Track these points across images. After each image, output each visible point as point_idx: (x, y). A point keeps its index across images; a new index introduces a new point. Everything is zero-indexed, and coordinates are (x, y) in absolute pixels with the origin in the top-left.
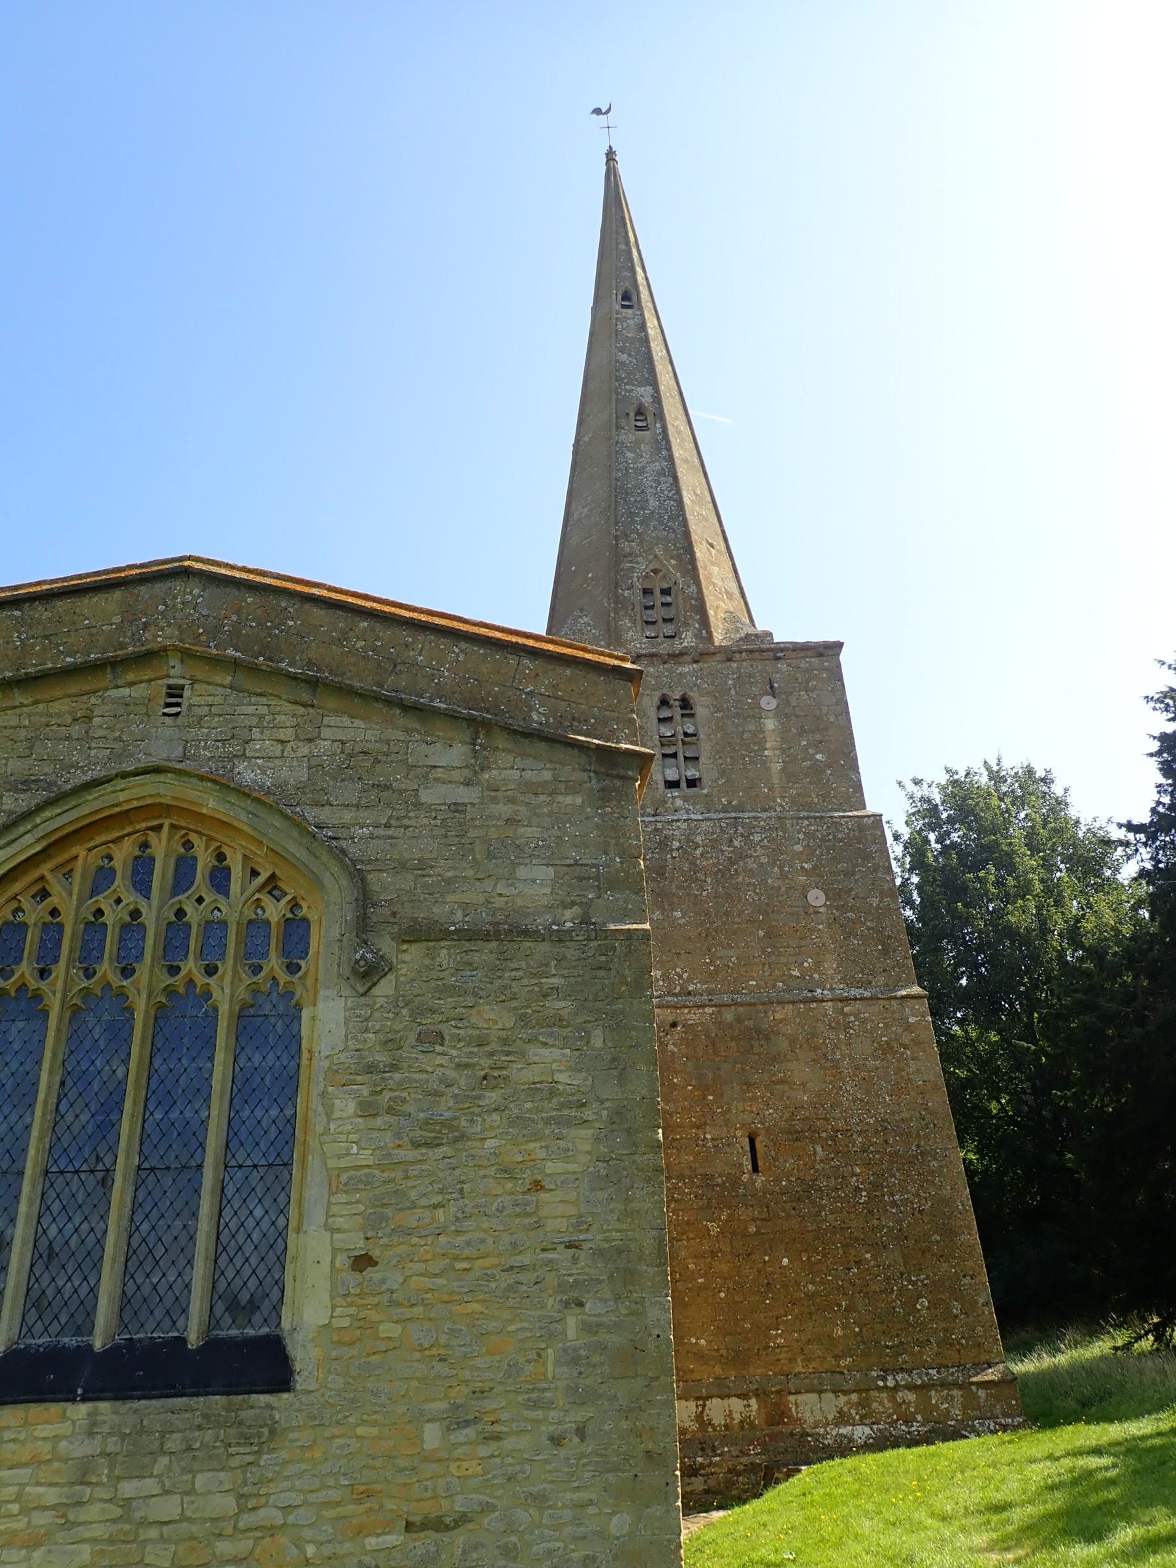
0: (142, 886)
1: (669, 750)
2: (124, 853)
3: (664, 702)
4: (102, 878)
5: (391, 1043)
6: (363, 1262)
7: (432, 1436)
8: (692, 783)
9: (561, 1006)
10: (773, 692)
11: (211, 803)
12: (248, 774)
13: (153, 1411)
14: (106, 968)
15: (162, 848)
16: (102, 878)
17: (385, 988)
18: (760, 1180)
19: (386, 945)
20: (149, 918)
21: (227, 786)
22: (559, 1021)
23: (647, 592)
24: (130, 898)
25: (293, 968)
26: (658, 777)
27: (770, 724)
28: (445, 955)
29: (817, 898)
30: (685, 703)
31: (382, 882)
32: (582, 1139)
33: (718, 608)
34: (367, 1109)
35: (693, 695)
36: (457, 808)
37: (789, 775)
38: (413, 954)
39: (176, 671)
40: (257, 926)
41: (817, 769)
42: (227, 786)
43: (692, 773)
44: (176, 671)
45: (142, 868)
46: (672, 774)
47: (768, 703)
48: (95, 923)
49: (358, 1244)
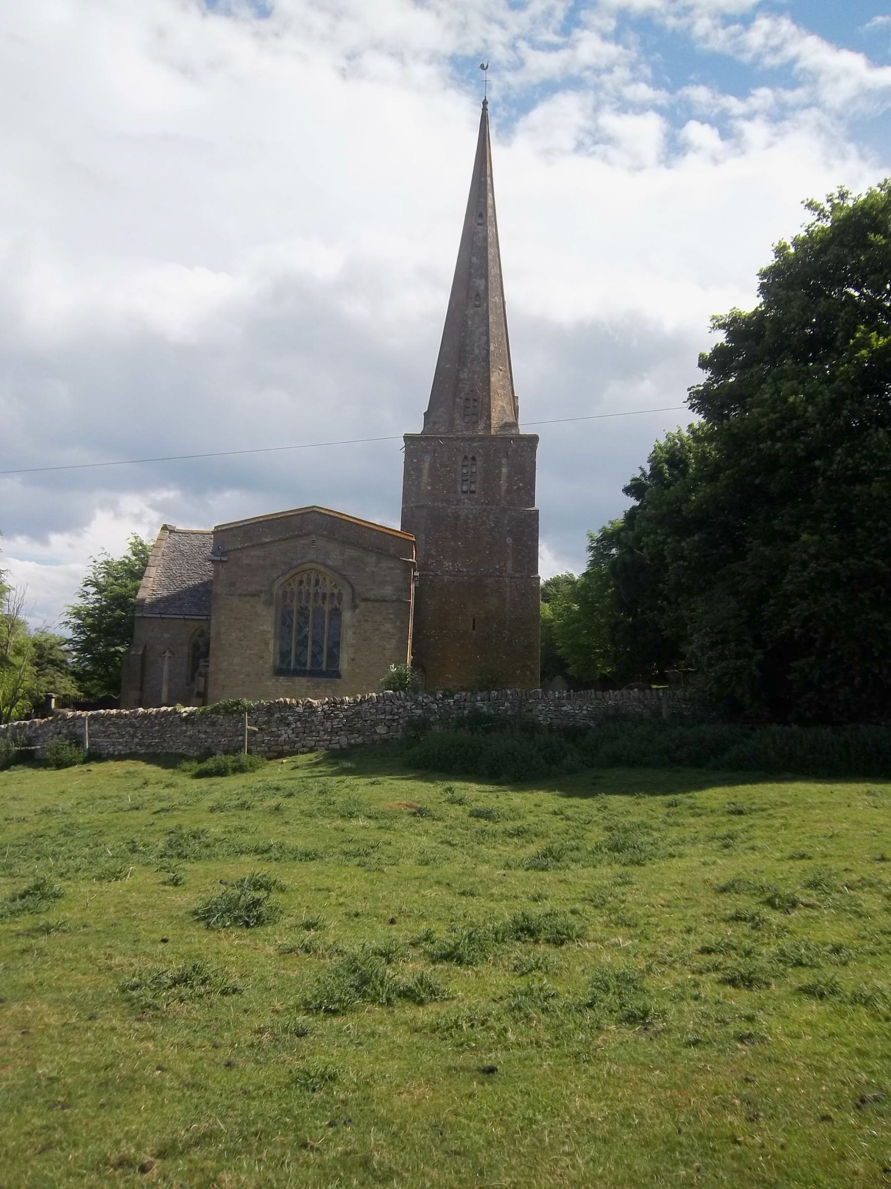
0: (309, 583)
1: (465, 478)
2: (305, 578)
3: (466, 458)
4: (301, 582)
5: (359, 621)
6: (353, 660)
7: (364, 687)
8: (473, 492)
9: (392, 616)
10: (507, 456)
11: (322, 569)
12: (330, 563)
13: (316, 679)
14: (304, 602)
15: (313, 577)
16: (301, 582)
17: (358, 611)
18: (474, 632)
19: (358, 602)
20: (311, 591)
21: (325, 565)
22: (391, 619)
23: (467, 400)
24: (307, 588)
25: (339, 603)
26: (459, 490)
27: (504, 470)
28: (370, 605)
29: (509, 540)
30: (473, 459)
31: (357, 588)
32: (394, 641)
33: (498, 405)
34: (354, 633)
35: (477, 456)
36: (373, 572)
37: (509, 491)
38: (363, 604)
39: (314, 537)
40: (333, 595)
41: (519, 489)
42: (325, 565)
43: (473, 487)
44: (314, 537)
45: (309, 580)
46: (465, 488)
47: (504, 461)
48: (300, 593)
49: (352, 656)
